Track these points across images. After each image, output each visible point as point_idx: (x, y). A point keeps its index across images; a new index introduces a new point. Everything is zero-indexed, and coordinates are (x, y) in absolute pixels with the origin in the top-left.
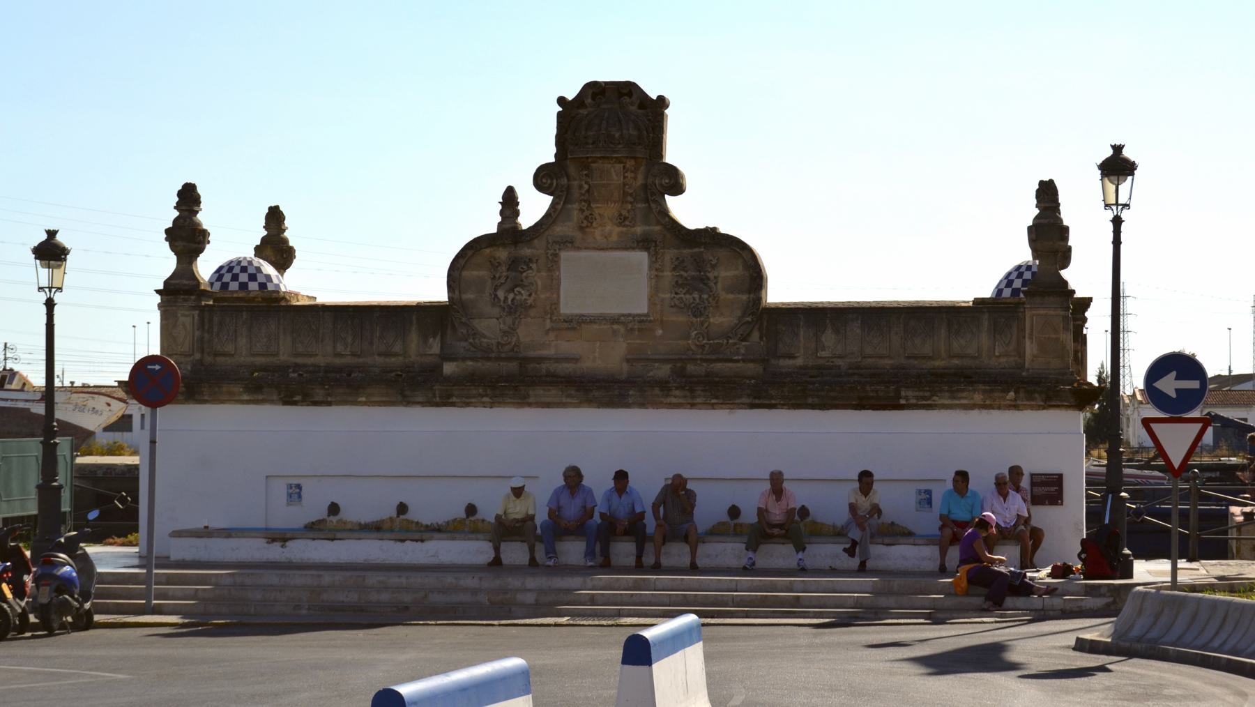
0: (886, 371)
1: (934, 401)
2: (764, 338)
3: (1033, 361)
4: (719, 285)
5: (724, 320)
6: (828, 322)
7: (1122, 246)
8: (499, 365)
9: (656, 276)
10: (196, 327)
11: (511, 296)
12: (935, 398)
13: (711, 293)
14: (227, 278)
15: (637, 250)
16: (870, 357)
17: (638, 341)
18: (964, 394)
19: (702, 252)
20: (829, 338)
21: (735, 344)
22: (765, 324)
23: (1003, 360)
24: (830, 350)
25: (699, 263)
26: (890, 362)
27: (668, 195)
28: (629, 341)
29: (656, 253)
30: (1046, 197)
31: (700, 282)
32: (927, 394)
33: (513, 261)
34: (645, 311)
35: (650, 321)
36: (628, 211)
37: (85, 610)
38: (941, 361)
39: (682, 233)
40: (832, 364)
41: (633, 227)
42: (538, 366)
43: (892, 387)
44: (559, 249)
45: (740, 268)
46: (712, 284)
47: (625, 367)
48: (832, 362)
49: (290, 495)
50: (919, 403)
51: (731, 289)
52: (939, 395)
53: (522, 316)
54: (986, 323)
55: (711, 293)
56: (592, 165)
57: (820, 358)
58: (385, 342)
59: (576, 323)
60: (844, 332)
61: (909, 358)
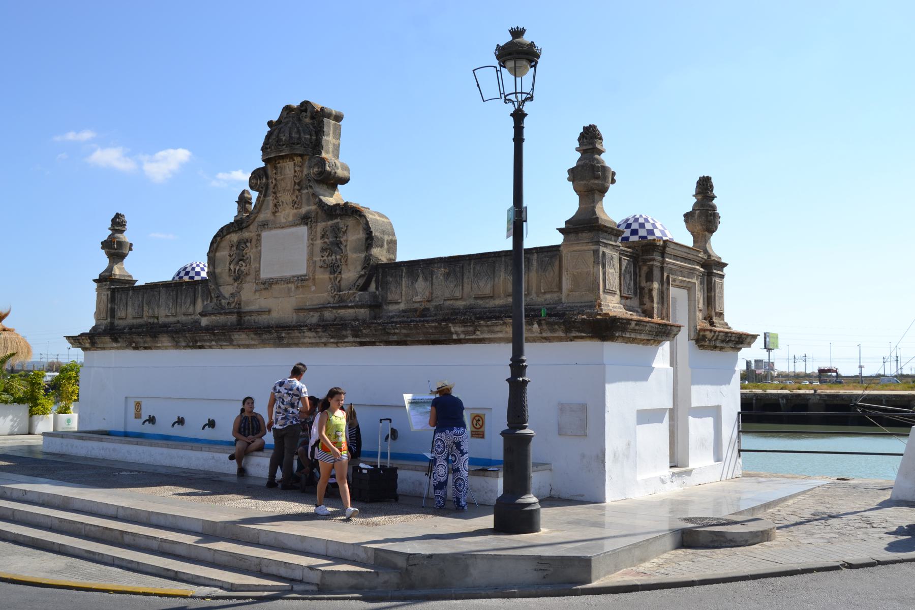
1: (477, 335)
3: (568, 295)
4: (348, 248)
7: (525, 145)
9: (311, 244)
12: (478, 333)
13: (342, 254)
14: (182, 274)
15: (302, 226)
16: (449, 300)
17: (301, 296)
18: (498, 328)
19: (338, 223)
20: (421, 284)
21: (354, 293)
22: (380, 277)
23: (548, 296)
24: (421, 295)
25: (336, 230)
26: (464, 303)
27: (340, 184)
28: (297, 296)
29: (311, 227)
30: (585, 140)
31: (334, 245)
32: (471, 329)
33: (239, 243)
35: (307, 280)
36: (297, 197)
38: (500, 300)
41: (300, 208)
42: (250, 318)
43: (443, 324)
44: (261, 231)
45: (361, 232)
46: (342, 247)
47: (295, 316)
50: (467, 337)
51: (356, 250)
52: (479, 329)
53: (243, 282)
54: (535, 263)
55: (342, 254)
56: (278, 165)
57: (416, 302)
59: (269, 284)
60: (430, 279)
61: (476, 298)
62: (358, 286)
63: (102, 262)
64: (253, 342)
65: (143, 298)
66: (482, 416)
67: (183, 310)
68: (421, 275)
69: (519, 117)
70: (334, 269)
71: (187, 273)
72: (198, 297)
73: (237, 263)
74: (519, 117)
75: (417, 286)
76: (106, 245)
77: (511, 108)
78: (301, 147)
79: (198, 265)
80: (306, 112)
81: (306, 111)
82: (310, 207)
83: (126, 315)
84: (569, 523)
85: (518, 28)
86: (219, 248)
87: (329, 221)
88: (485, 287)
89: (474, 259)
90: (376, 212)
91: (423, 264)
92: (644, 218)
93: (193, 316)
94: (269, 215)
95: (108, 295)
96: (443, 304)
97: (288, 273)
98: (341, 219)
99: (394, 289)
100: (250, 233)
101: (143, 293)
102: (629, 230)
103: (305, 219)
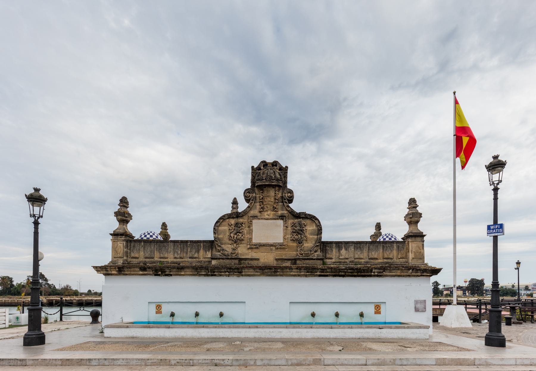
14: (143, 236)
19: (301, 221)
20: (343, 251)
26: (364, 260)
51: (312, 234)
56: (264, 189)
59: (259, 246)
63: (115, 225)
64: (256, 273)
65: (155, 247)
66: (380, 305)
67: (189, 255)
69: (496, 190)
70: (300, 242)
71: (145, 236)
72: (200, 249)
74: (496, 190)
75: (342, 252)
76: (117, 214)
77: (493, 187)
79: (151, 232)
80: (276, 166)
81: (276, 166)
82: (284, 212)
83: (139, 255)
84: (58, 350)
85: (495, 155)
86: (221, 225)
87: (295, 219)
88: (358, 254)
89: (368, 243)
90: (219, 219)
91: (344, 243)
92: (156, 236)
93: (197, 259)
94: (257, 212)
95: (124, 243)
96: (354, 260)
97: (271, 241)
98: (302, 220)
99: (330, 253)
101: (155, 245)
102: (383, 239)
103: (282, 217)
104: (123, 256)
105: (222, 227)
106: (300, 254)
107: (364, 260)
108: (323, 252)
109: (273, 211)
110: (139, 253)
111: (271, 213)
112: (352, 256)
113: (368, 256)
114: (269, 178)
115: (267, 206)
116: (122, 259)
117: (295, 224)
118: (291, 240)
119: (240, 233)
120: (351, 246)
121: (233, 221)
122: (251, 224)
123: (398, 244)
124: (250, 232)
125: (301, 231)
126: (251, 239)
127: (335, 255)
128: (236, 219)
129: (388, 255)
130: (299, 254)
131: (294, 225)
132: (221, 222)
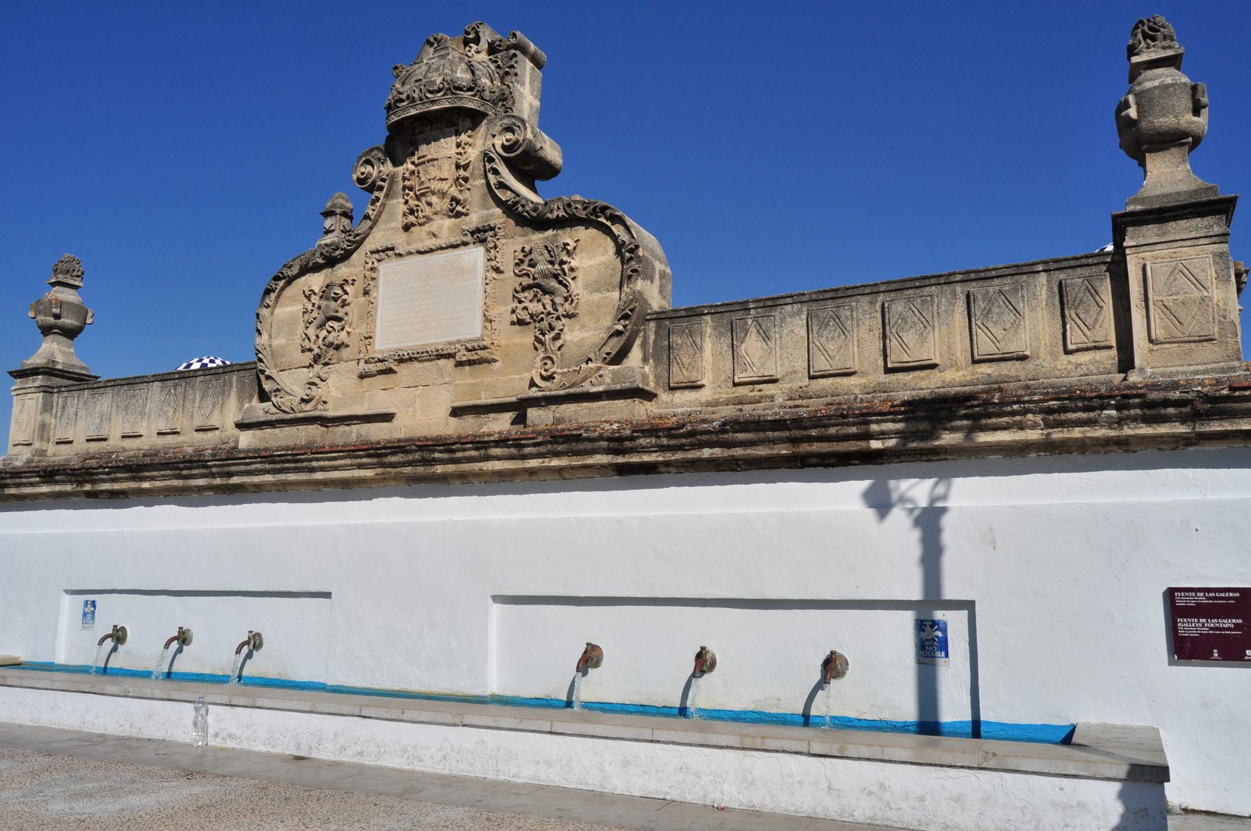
0: (853, 397)
2: (651, 361)
5: (586, 334)
6: (750, 321)
7: (1196, 809)
8: (298, 429)
10: (39, 411)
11: (323, 333)
21: (599, 368)
26: (863, 381)
32: (924, 426)
34: (479, 335)
37: (931, 615)
38: (957, 370)
39: (527, 208)
40: (759, 394)
48: (760, 390)
49: (85, 614)
51: (596, 287)
56: (418, 136)
58: (203, 412)
62: (608, 354)
68: (753, 330)
73: (321, 326)
78: (474, 96)
80: (477, 44)
93: (217, 433)
99: (686, 360)
100: (352, 269)
103: (481, 235)
104: (33, 438)
105: (286, 306)
106: (543, 378)
107: (863, 381)
108: (658, 362)
109: (450, 217)
110: (75, 425)
111: (445, 227)
112: (801, 364)
113: (885, 356)
114: (421, 90)
115: (429, 199)
116: (30, 448)
117: (530, 252)
118: (513, 323)
119: (339, 319)
120: (793, 315)
121: (316, 281)
122: (373, 279)
123: (1062, 276)
124: (368, 315)
125: (556, 276)
126: (370, 338)
127: (716, 370)
128: (327, 271)
129: (995, 340)
130: (538, 381)
131: (526, 258)
132: (279, 288)
